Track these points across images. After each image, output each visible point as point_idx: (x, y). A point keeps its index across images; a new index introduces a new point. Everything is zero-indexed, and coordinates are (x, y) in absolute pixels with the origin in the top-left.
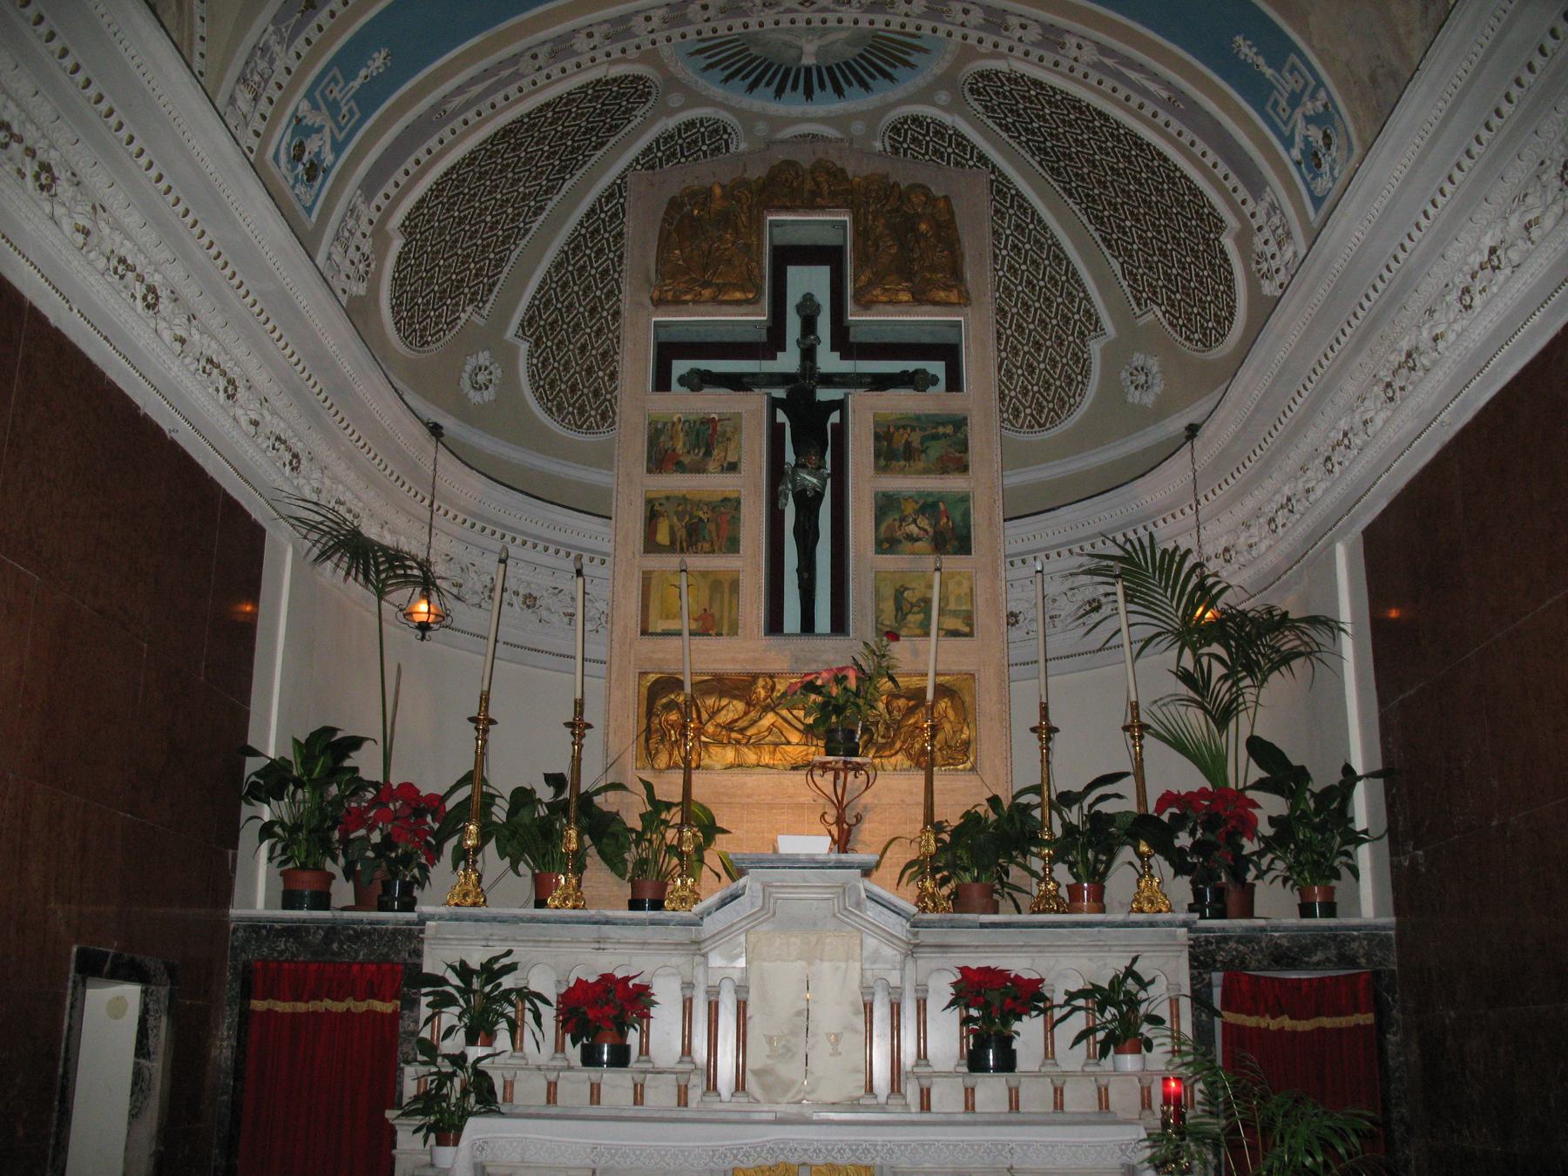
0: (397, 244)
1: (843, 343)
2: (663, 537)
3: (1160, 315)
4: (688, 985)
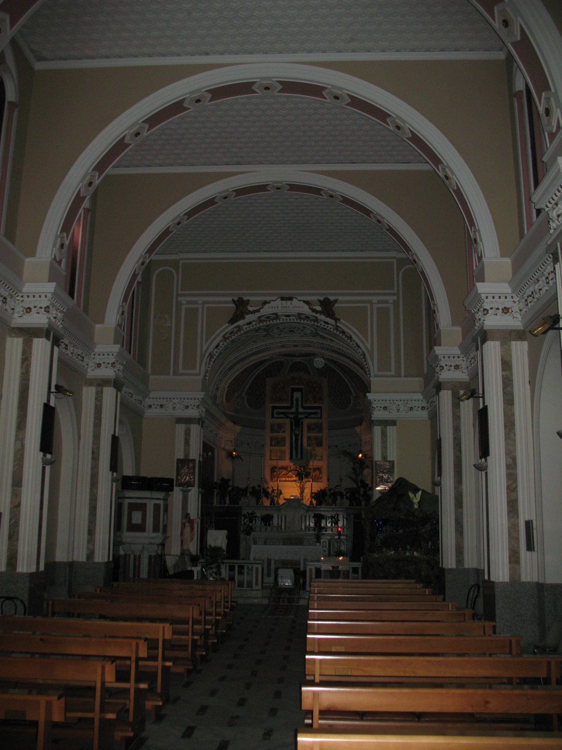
0: (227, 389)
2: (273, 444)
4: (278, 515)
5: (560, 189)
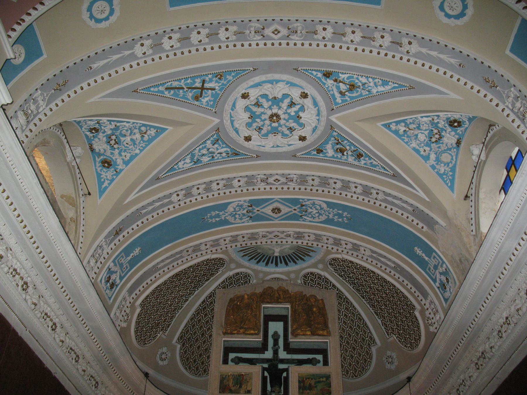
0: (138, 310)
1: (287, 348)
3: (395, 338)
5: (525, 237)
